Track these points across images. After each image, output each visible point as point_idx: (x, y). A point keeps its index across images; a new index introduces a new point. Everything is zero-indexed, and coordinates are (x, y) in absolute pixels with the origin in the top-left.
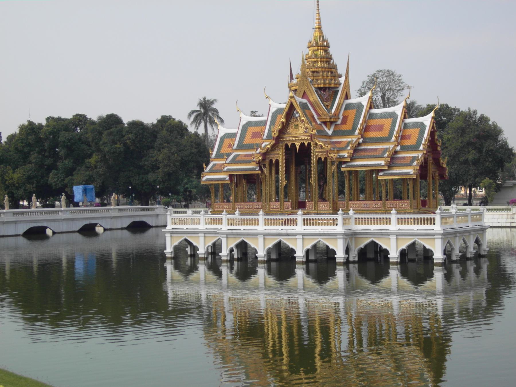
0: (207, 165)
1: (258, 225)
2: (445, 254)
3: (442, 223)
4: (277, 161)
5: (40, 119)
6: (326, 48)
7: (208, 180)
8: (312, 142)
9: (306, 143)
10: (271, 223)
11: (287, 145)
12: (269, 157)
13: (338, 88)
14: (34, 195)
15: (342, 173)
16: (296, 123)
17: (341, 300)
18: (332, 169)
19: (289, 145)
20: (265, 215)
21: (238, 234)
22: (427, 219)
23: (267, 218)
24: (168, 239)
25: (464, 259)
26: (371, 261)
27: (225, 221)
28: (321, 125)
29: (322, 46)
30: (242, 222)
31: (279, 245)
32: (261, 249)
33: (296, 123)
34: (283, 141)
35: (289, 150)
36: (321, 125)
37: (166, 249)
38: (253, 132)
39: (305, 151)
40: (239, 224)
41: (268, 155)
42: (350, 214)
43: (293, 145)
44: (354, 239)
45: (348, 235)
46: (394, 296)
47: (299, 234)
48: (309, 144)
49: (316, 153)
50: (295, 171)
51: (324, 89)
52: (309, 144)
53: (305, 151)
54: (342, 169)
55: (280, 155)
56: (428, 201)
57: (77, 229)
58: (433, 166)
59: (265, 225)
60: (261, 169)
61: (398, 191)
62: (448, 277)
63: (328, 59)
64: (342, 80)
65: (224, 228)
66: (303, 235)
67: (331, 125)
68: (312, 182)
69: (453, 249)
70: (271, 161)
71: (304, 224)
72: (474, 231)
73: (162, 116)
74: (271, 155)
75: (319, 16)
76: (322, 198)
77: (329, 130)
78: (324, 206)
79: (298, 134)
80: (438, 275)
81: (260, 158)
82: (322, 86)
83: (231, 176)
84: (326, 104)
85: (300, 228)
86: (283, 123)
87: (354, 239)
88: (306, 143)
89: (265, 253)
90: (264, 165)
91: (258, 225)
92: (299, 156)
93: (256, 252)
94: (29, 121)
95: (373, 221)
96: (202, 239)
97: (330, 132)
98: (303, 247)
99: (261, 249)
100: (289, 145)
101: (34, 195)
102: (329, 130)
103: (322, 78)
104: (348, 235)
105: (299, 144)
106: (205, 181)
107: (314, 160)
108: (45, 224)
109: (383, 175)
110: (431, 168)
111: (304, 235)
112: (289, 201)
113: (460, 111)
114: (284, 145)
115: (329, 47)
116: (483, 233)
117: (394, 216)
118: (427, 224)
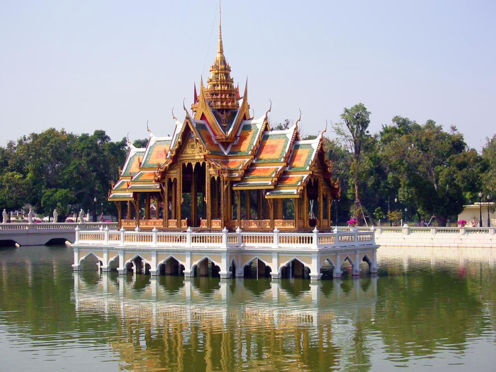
0: (116, 182)
3: (227, 241)
4: (175, 179)
6: (226, 70)
7: (114, 197)
8: (206, 162)
11: (184, 165)
12: (168, 176)
13: (236, 110)
15: (233, 192)
16: (192, 144)
17: (314, 313)
18: (224, 187)
19: (186, 165)
20: (158, 231)
21: (133, 250)
24: (76, 255)
25: (346, 274)
26: (254, 276)
27: (276, 239)
28: (218, 145)
29: (223, 70)
31: (206, 261)
33: (192, 144)
34: (181, 160)
35: (187, 169)
36: (218, 145)
37: (118, 267)
39: (201, 169)
41: (167, 173)
43: (190, 164)
45: (233, 253)
46: (273, 310)
48: (204, 164)
49: (211, 172)
51: (221, 110)
52: (204, 164)
53: (201, 169)
54: (234, 189)
55: (176, 174)
56: (318, 221)
57: (44, 244)
58: (324, 187)
59: (158, 241)
60: (161, 187)
61: (285, 210)
62: (232, 288)
63: (228, 81)
65: (121, 244)
68: (206, 201)
70: (170, 179)
72: (361, 250)
75: (221, 37)
76: (216, 215)
77: (226, 150)
78: (216, 224)
79: (196, 154)
81: (159, 177)
82: (219, 107)
83: (135, 194)
84: (224, 125)
86: (179, 143)
89: (158, 269)
90: (164, 184)
91: (104, 239)
92: (194, 176)
93: (309, 271)
100: (186, 165)
101: (5, 210)
102: (226, 150)
104: (233, 253)
105: (195, 163)
106: (111, 198)
107: (208, 181)
109: (269, 195)
110: (322, 189)
112: (185, 219)
114: (182, 164)
115: (230, 71)
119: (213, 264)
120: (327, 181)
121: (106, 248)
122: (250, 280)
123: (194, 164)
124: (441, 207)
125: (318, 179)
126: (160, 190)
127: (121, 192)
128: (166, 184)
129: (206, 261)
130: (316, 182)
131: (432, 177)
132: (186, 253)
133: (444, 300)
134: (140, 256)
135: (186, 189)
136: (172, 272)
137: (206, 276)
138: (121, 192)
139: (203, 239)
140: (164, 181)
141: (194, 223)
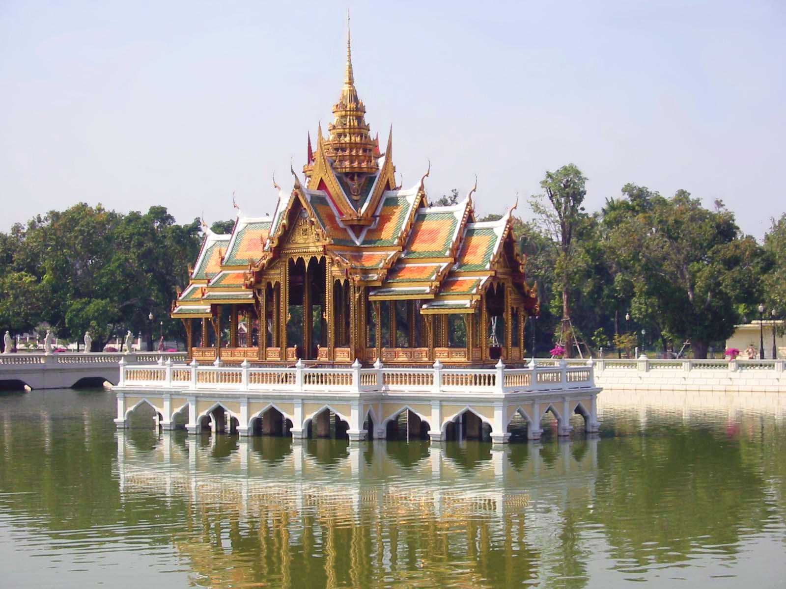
0: (183, 289)
2: (508, 431)
3: (360, 382)
4: (278, 284)
5: (93, 205)
6: (358, 111)
7: (181, 312)
12: (266, 279)
14: (7, 332)
15: (369, 304)
16: (304, 227)
18: (355, 297)
19: (295, 261)
21: (212, 396)
24: (120, 403)
26: (403, 437)
27: (355, 378)
31: (326, 413)
33: (304, 227)
35: (296, 268)
37: (187, 422)
39: (318, 268)
41: (265, 275)
42: (376, 368)
43: (301, 260)
46: (433, 492)
48: (323, 259)
49: (334, 272)
50: (310, 298)
51: (351, 175)
52: (323, 259)
53: (318, 268)
54: (371, 298)
55: (279, 276)
57: (70, 386)
58: (513, 296)
60: (255, 297)
61: (452, 332)
62: (368, 456)
63: (361, 129)
64: (381, 161)
68: (327, 318)
69: (528, 424)
70: (269, 284)
71: (306, 382)
74: (269, 275)
75: (350, 58)
76: (342, 340)
77: (358, 237)
78: (343, 354)
79: (310, 244)
80: (354, 454)
81: (252, 279)
82: (348, 170)
83: (214, 307)
84: (355, 198)
86: (284, 226)
89: (443, 430)
90: (260, 291)
91: (164, 379)
92: (307, 279)
94: (628, 189)
96: (436, 412)
100: (295, 261)
101: (7, 332)
102: (358, 237)
105: (309, 259)
107: (329, 286)
108: (21, 377)
109: (427, 309)
110: (511, 299)
112: (294, 347)
114: (288, 259)
116: (591, 399)
118: (453, 384)
119: (337, 417)
120: (519, 287)
121: (167, 392)
122: (396, 444)
123: (307, 260)
124: (699, 328)
125: (503, 284)
126: (253, 302)
127: (192, 304)
128: (264, 292)
129: (326, 413)
130: (501, 289)
131: (684, 280)
132: (295, 401)
133: (703, 474)
134: (221, 405)
135: (295, 298)
137: (327, 436)
138: (192, 304)
139: (321, 379)
140: (259, 287)
141: (308, 354)
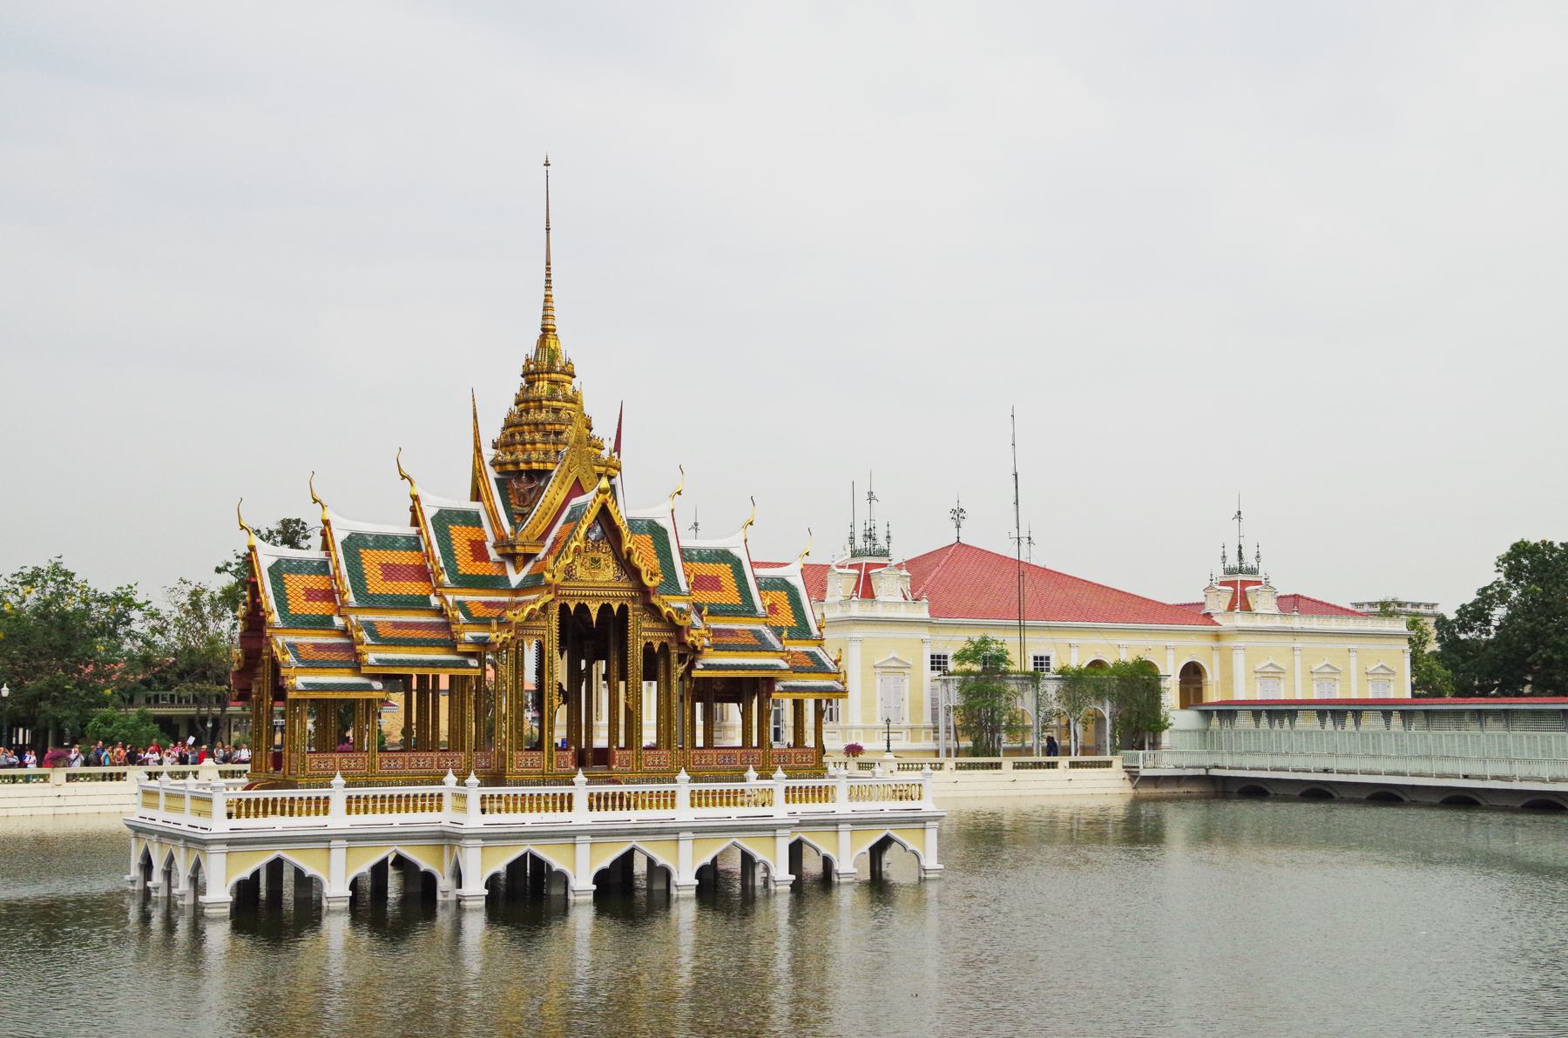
1: (673, 806)
9: (615, 607)
10: (300, 809)
22: (266, 800)
23: (354, 795)
29: (545, 372)
30: (239, 808)
32: (581, 871)
38: (385, 580)
40: (499, 811)
43: (582, 609)
44: (446, 849)
47: (845, 821)
66: (351, 838)
67: (525, 563)
71: (349, 812)
73: (1527, 561)
85: (581, 816)
87: (446, 849)
88: (615, 607)
95: (419, 804)
97: (515, 578)
98: (228, 875)
99: (581, 871)
103: (540, 444)
111: (353, 838)
113: (1557, 544)
117: (338, 792)
134: (284, 855)
136: (526, 896)
